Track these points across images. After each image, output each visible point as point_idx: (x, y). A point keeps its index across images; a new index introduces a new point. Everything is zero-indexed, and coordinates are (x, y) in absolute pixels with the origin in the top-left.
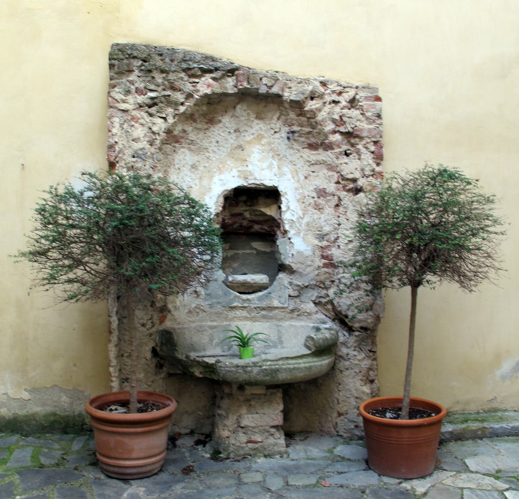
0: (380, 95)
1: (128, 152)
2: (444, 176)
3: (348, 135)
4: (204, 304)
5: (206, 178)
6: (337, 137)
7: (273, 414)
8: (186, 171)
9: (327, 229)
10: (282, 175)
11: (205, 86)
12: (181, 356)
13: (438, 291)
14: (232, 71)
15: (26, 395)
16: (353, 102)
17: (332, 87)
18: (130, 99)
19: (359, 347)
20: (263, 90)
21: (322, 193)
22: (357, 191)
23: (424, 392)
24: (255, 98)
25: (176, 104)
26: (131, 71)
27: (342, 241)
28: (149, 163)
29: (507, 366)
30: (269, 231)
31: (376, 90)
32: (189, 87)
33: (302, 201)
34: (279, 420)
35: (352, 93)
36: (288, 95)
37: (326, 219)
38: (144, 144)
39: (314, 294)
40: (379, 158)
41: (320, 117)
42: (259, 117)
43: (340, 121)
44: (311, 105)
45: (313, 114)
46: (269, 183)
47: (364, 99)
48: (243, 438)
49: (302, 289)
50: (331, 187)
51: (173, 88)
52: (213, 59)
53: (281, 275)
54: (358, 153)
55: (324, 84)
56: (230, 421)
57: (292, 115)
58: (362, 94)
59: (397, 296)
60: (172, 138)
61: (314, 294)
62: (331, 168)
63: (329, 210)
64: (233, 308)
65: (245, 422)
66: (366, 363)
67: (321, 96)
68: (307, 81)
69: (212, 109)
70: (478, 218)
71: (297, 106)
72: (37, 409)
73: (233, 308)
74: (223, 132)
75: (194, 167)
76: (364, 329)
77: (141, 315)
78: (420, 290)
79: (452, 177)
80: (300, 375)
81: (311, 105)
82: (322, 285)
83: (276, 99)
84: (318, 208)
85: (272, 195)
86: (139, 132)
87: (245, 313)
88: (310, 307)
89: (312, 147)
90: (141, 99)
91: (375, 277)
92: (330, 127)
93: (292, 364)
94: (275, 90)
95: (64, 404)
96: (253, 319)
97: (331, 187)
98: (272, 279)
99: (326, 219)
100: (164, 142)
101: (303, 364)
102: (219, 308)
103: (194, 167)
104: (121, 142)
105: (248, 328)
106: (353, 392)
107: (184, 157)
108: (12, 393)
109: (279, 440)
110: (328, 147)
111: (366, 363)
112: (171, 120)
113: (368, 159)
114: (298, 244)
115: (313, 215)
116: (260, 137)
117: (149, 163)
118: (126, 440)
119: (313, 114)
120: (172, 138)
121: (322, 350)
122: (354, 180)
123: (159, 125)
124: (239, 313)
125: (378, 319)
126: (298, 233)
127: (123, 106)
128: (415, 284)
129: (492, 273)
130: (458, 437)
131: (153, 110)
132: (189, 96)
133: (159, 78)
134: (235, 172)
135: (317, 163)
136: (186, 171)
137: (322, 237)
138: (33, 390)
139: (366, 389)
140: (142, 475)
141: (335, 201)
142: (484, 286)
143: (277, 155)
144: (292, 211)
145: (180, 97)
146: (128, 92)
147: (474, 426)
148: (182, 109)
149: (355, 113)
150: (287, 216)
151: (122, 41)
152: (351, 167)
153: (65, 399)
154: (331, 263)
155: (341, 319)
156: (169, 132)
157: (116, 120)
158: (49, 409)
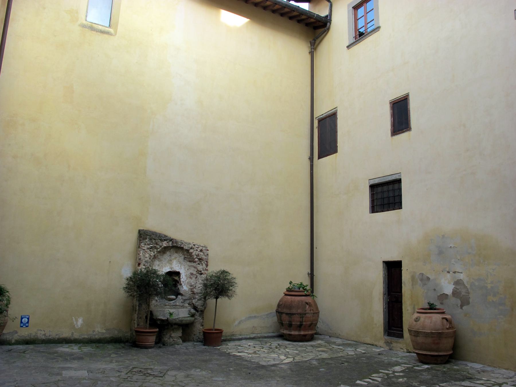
0: (208, 249)
1: (144, 261)
2: (224, 272)
3: (200, 259)
4: (159, 304)
5: (163, 268)
6: (197, 260)
7: (179, 333)
8: (157, 266)
9: (193, 284)
10: (181, 268)
11: (165, 244)
12: (155, 318)
13: (222, 300)
14: (171, 240)
15: (104, 331)
16: (201, 251)
17: (196, 246)
18: (146, 246)
19: (200, 316)
20: (179, 246)
21: (192, 274)
22: (201, 274)
23: (216, 327)
24: (176, 247)
25: (157, 249)
26: (146, 239)
27: (197, 287)
28: (149, 264)
29: (237, 323)
30: (177, 283)
31: (207, 247)
32: (161, 244)
33: (186, 276)
34: (181, 335)
35: (201, 248)
36: (186, 247)
37: (193, 281)
38: (148, 259)
39: (188, 302)
40: (207, 265)
41: (193, 254)
42: (176, 252)
43: (198, 255)
44: (191, 251)
45: (192, 253)
46: (177, 271)
47: (204, 250)
48: (172, 340)
49: (185, 300)
50: (195, 273)
51: (157, 244)
52: (166, 236)
53: (179, 296)
54: (202, 264)
55: (194, 245)
56: (168, 336)
57: (185, 253)
58: (204, 249)
59: (211, 301)
60: (155, 257)
61: (188, 302)
62: (195, 267)
63: (194, 279)
64: (166, 305)
65: (172, 336)
66: (202, 320)
67: (194, 248)
68: (190, 244)
69: (165, 250)
70: (232, 283)
71: (188, 251)
72: (107, 336)
73: (166, 305)
74: (167, 256)
75: (159, 265)
76: (201, 311)
77: (144, 306)
78: (218, 300)
79: (227, 272)
80: (188, 322)
81: (191, 251)
82: (190, 299)
83: (182, 248)
84: (191, 278)
85: (178, 274)
86: (147, 255)
87: (169, 307)
88: (187, 305)
89: (190, 261)
90: (148, 247)
91: (205, 297)
92: (195, 257)
93: (186, 319)
94: (182, 246)
95: (116, 334)
96: (171, 309)
97: (195, 273)
98: (177, 297)
99: (193, 281)
100: (153, 258)
101: (188, 319)
102: (162, 305)
103: (159, 265)
104: (142, 258)
105: (172, 311)
106: (198, 329)
107: (157, 262)
108: (100, 330)
109: (180, 341)
110: (195, 262)
111: (202, 320)
112: (155, 253)
113: (204, 265)
114: (185, 288)
115: (189, 280)
116: (176, 258)
117: (149, 264)
118: (148, 337)
119: (192, 253)
120: (155, 257)
121: (193, 315)
122: (201, 271)
123: (152, 254)
124: (167, 307)
125: (205, 308)
126: (185, 285)
127: (144, 248)
128: (217, 298)
129: (235, 295)
130: (225, 340)
131: (151, 250)
132: (161, 246)
133: (154, 241)
134: (169, 267)
135: (191, 266)
136: (157, 266)
137: (191, 286)
138: (107, 330)
139: (201, 328)
140: (151, 348)
141: (195, 276)
142: (233, 299)
143: (180, 263)
144: (183, 278)
145: (158, 247)
146: (145, 245)
147: (228, 338)
148: (159, 250)
149: (202, 253)
150: (182, 280)
151: (142, 229)
152: (200, 268)
153: (116, 332)
154: (193, 293)
155: (195, 308)
156: (154, 256)
157: (141, 252)
158: (111, 335)
